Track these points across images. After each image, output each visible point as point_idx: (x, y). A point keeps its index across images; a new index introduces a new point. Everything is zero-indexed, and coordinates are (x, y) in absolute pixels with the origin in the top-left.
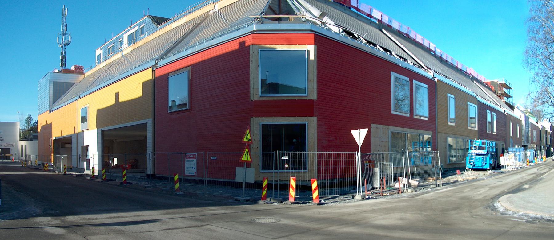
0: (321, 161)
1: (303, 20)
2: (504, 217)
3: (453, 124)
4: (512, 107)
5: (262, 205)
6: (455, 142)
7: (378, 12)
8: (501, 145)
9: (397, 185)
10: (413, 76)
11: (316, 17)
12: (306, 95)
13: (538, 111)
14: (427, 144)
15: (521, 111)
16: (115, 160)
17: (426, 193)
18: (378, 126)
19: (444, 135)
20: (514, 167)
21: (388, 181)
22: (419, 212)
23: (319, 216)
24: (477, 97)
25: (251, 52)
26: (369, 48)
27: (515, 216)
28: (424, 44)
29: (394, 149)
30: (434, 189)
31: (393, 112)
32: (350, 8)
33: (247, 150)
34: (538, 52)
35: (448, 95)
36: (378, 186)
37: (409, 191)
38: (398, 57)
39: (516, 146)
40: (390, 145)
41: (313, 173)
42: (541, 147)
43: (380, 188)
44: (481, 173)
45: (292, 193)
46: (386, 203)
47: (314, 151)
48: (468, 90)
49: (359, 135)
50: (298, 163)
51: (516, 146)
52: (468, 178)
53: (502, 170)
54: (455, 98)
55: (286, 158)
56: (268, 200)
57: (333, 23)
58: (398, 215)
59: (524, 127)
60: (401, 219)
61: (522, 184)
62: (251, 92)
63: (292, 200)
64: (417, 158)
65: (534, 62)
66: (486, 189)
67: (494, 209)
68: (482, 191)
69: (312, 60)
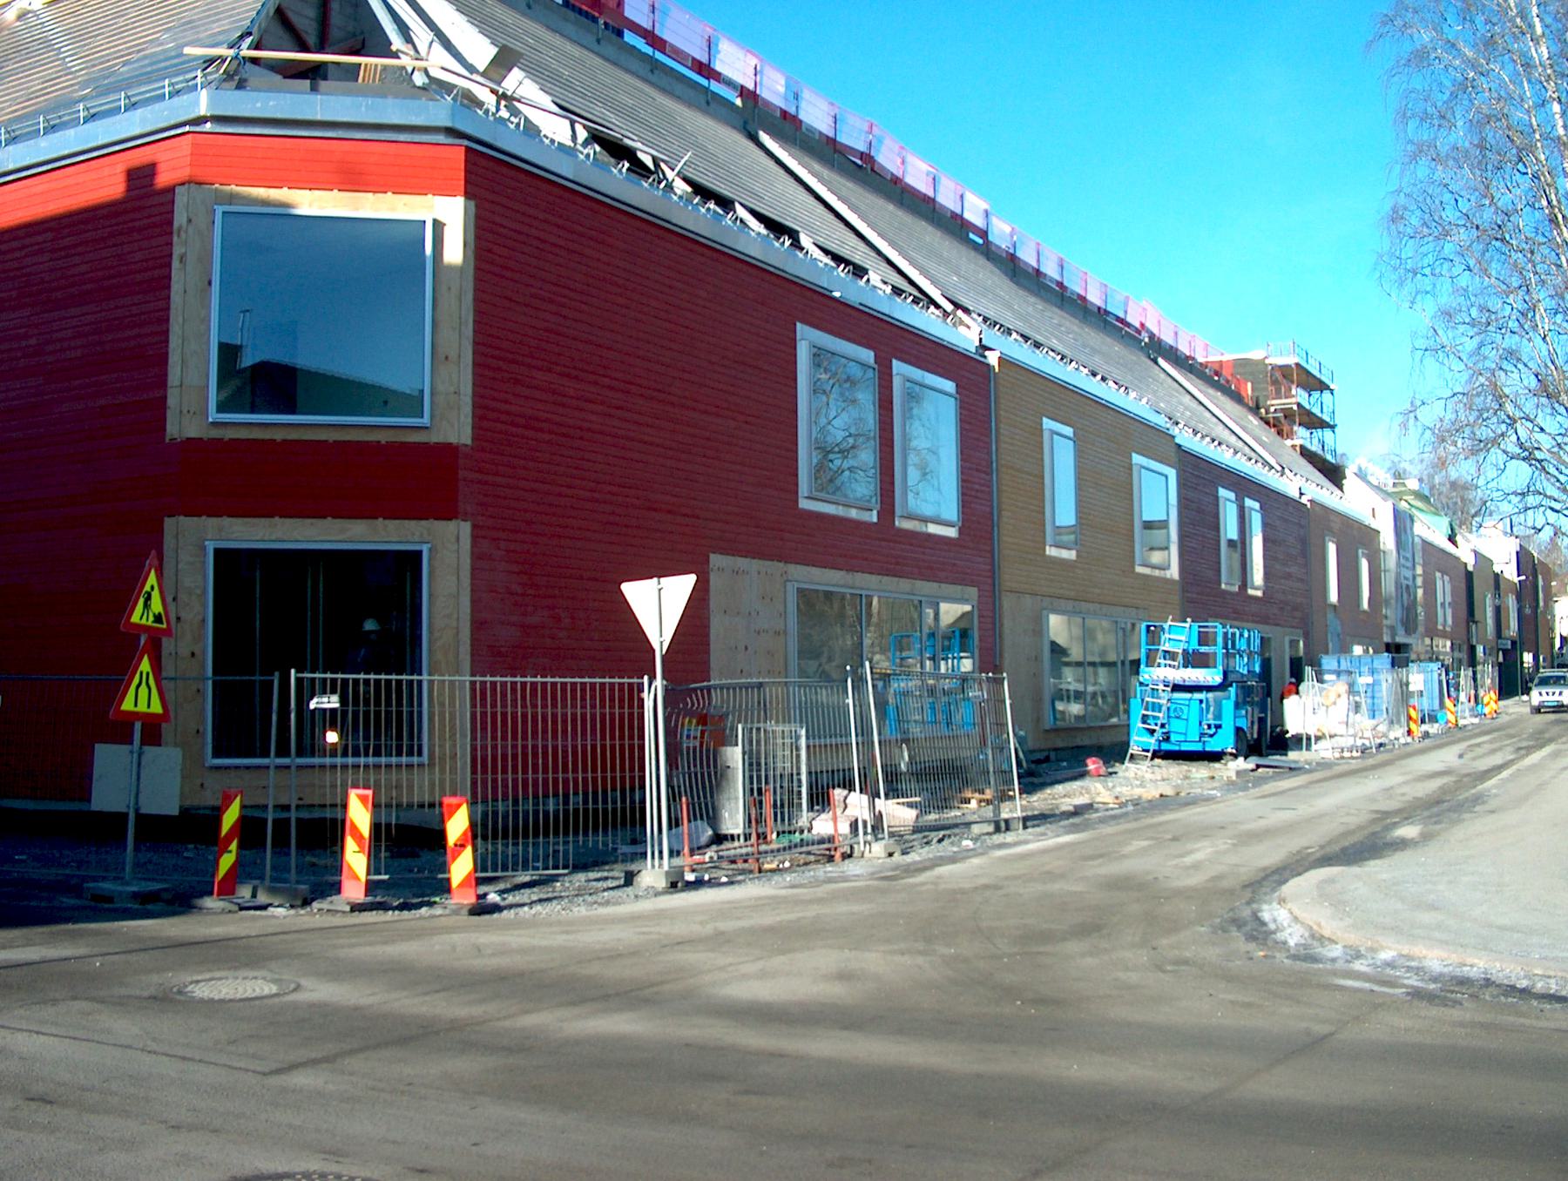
0: (488, 715)
1: (419, 79)
2: (1305, 972)
3: (1070, 555)
4: (1334, 474)
5: (214, 919)
6: (1077, 631)
7: (741, 54)
8: (1287, 643)
9: (822, 825)
10: (893, 341)
11: (471, 68)
12: (426, 420)
13: (1454, 485)
14: (956, 642)
15: (1378, 488)
16: (370, 625)
17: (953, 859)
18: (742, 563)
19: (1028, 601)
20: (1350, 742)
21: (786, 809)
22: (921, 946)
23: (478, 963)
24: (1175, 431)
25: (180, 219)
26: (700, 219)
27: (1359, 966)
28: (941, 199)
29: (812, 665)
30: (989, 841)
31: (804, 504)
32: (620, 34)
33: (145, 666)
34: (1450, 214)
35: (1048, 424)
36: (739, 830)
37: (878, 849)
38: (827, 260)
39: (1358, 650)
40: (793, 646)
41: (453, 770)
42: (1472, 649)
43: (747, 837)
44: (1199, 771)
45: (356, 859)
46: (775, 902)
47: (458, 672)
48: (1134, 403)
49: (657, 604)
50: (385, 728)
51: (1358, 650)
52: (1138, 792)
53: (1293, 755)
54: (1076, 439)
55: (331, 702)
56: (244, 892)
57: (546, 101)
58: (826, 959)
59: (1391, 561)
60: (843, 976)
61: (1387, 819)
62: (172, 401)
63: (354, 891)
64: (913, 704)
65: (1430, 259)
66: (1222, 843)
67: (1259, 932)
68: (1202, 851)
69: (451, 268)
